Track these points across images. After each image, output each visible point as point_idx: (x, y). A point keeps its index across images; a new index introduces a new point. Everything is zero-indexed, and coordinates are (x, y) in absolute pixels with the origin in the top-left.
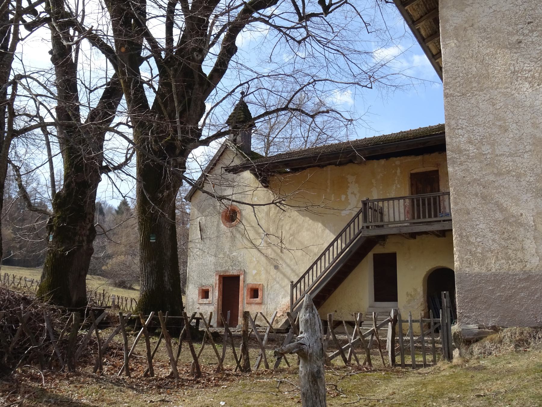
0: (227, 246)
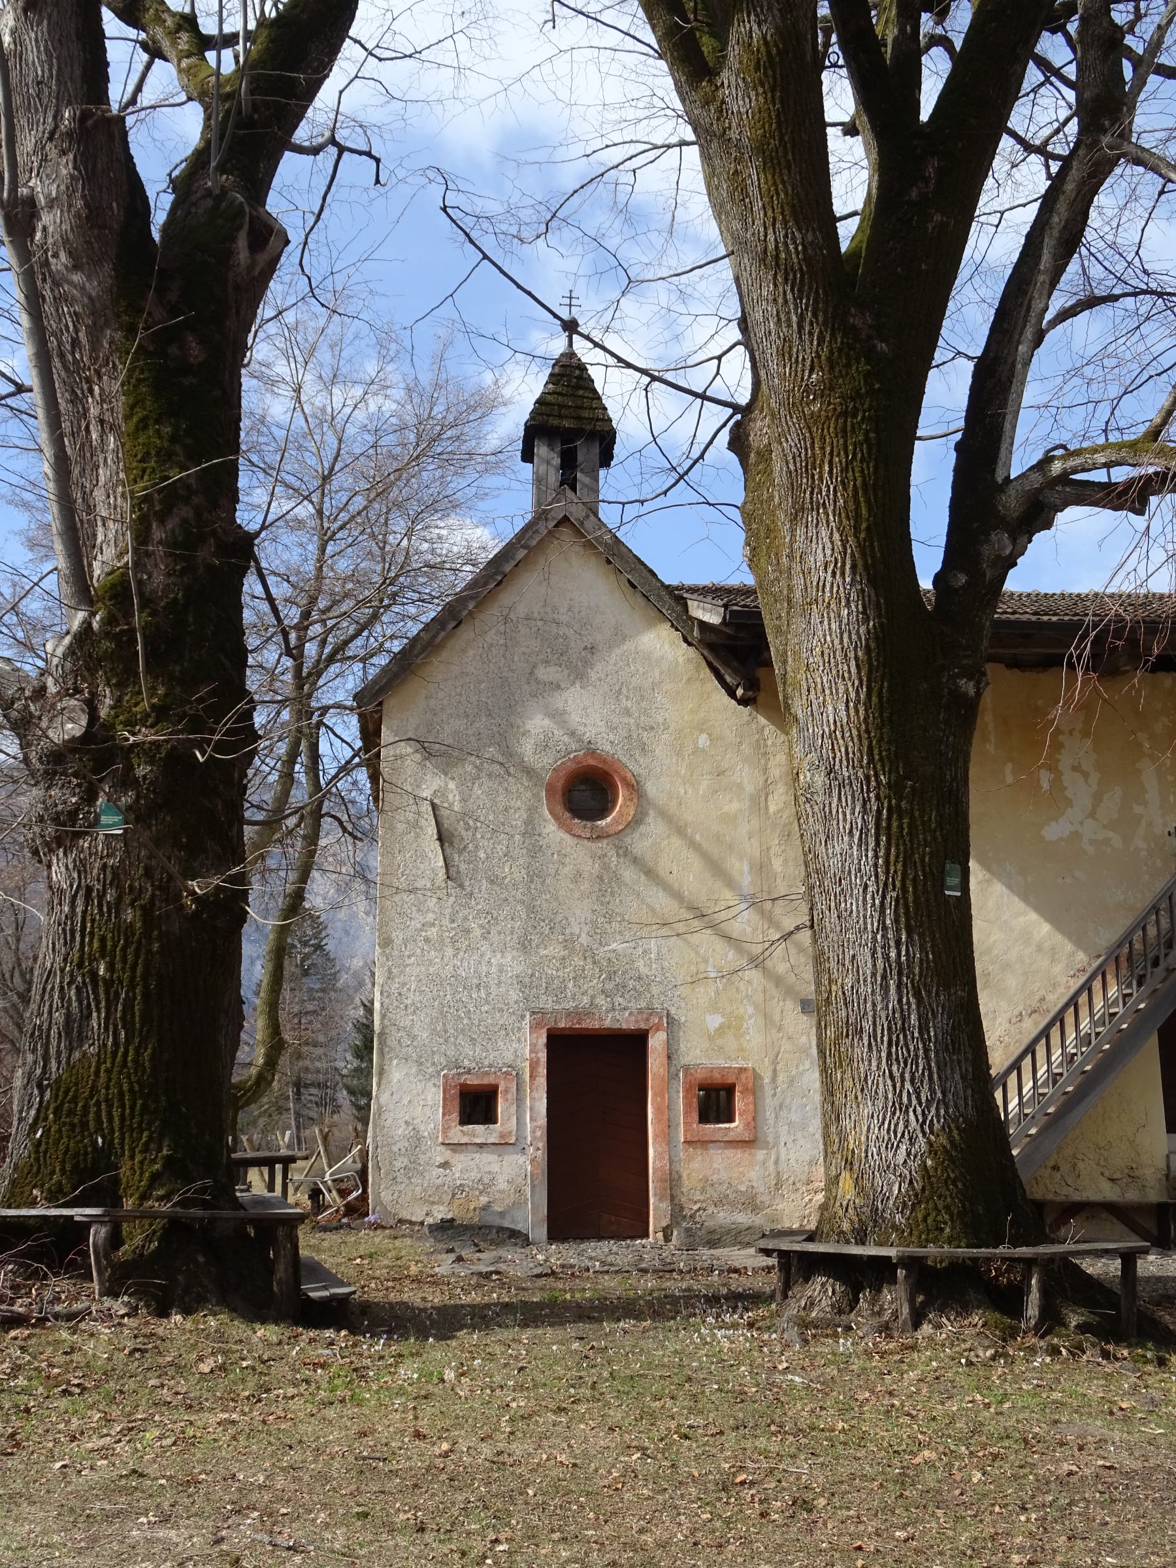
0: (579, 914)
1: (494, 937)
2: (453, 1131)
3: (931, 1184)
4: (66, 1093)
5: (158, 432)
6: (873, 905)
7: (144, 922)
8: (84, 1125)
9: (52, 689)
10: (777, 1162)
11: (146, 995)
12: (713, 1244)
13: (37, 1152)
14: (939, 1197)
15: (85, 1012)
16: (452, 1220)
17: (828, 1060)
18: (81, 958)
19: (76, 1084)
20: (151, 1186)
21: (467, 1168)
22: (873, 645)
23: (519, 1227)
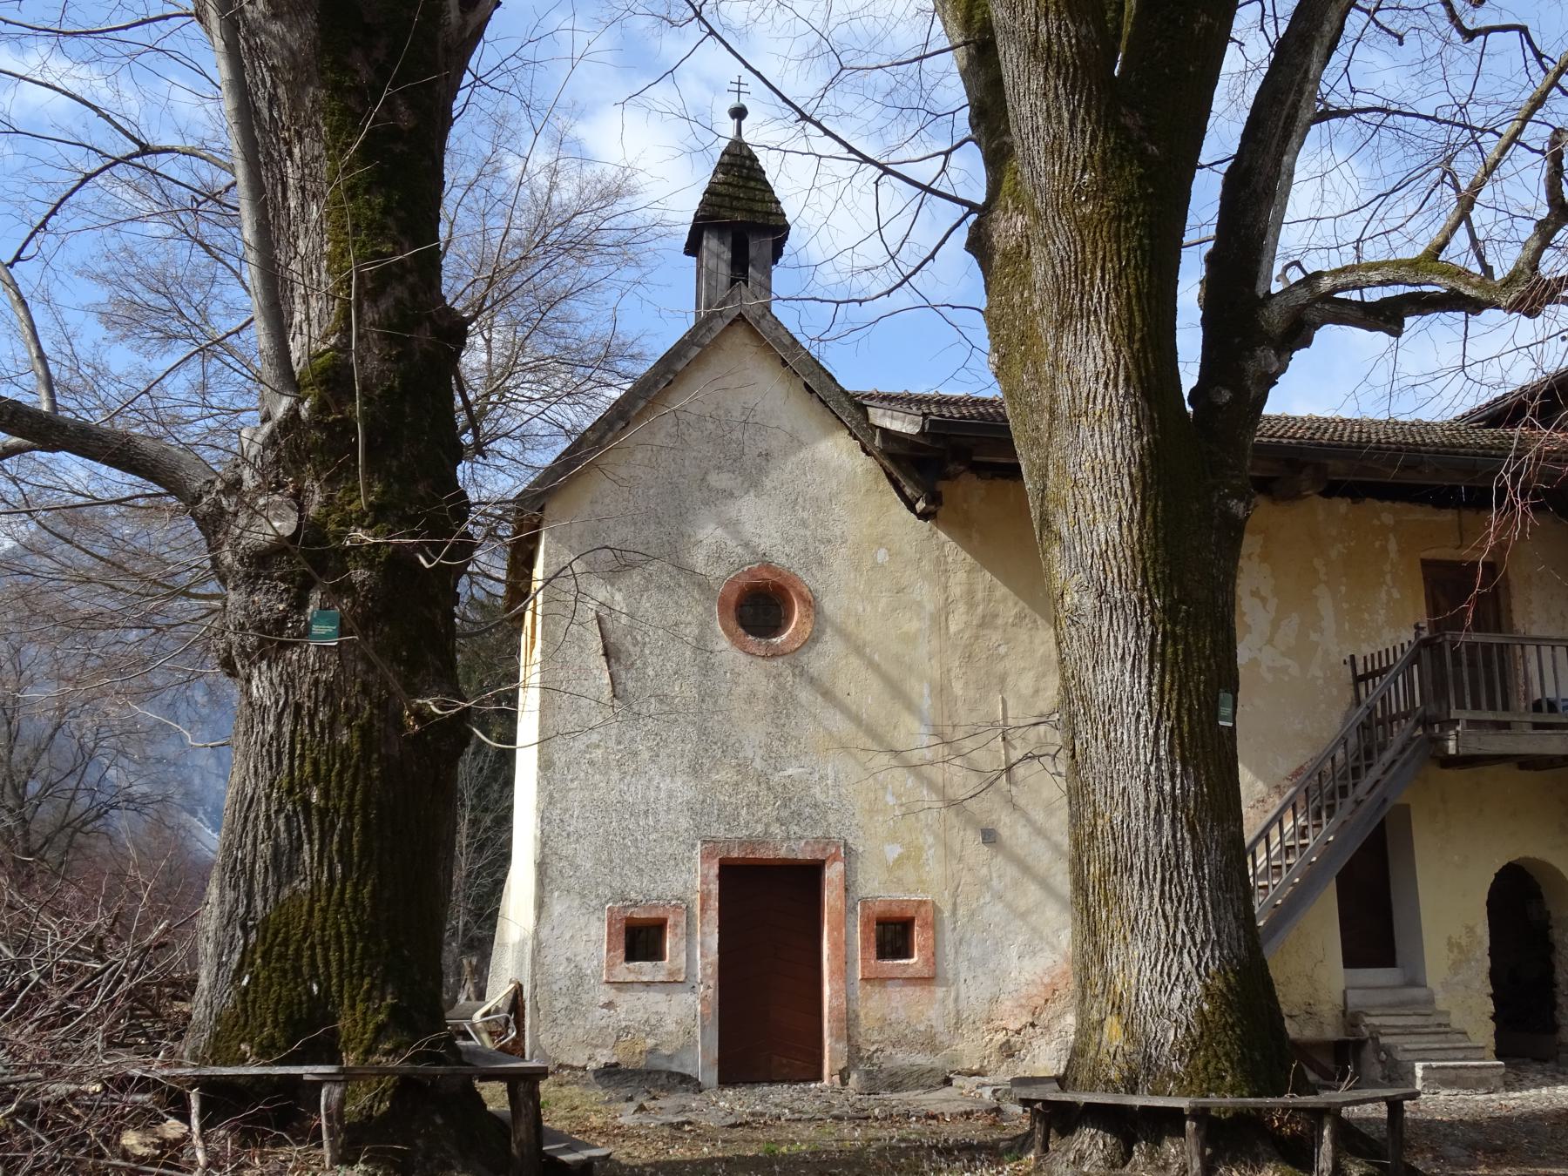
0: (753, 736)
1: (664, 761)
2: (618, 968)
3: (1209, 1029)
4: (276, 935)
5: (368, 202)
6: (1147, 735)
7: (363, 743)
8: (297, 971)
9: (249, 479)
10: (956, 1000)
11: (365, 825)
12: (895, 1087)
13: (244, 1002)
14: (1219, 1043)
15: (295, 843)
16: (617, 1064)
17: (1091, 898)
18: (291, 783)
19: (287, 925)
20: (376, 1040)
21: (635, 1008)
22: (1147, 462)
23: (688, 1071)
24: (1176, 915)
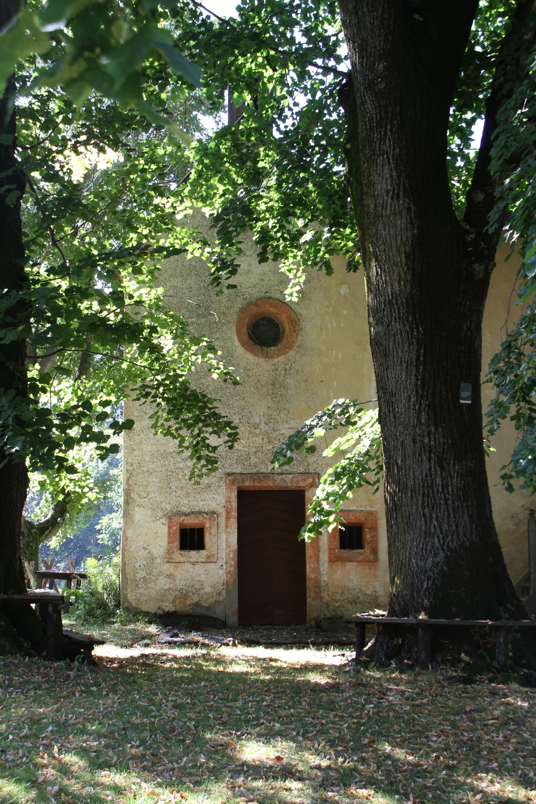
24: (431, 515)
